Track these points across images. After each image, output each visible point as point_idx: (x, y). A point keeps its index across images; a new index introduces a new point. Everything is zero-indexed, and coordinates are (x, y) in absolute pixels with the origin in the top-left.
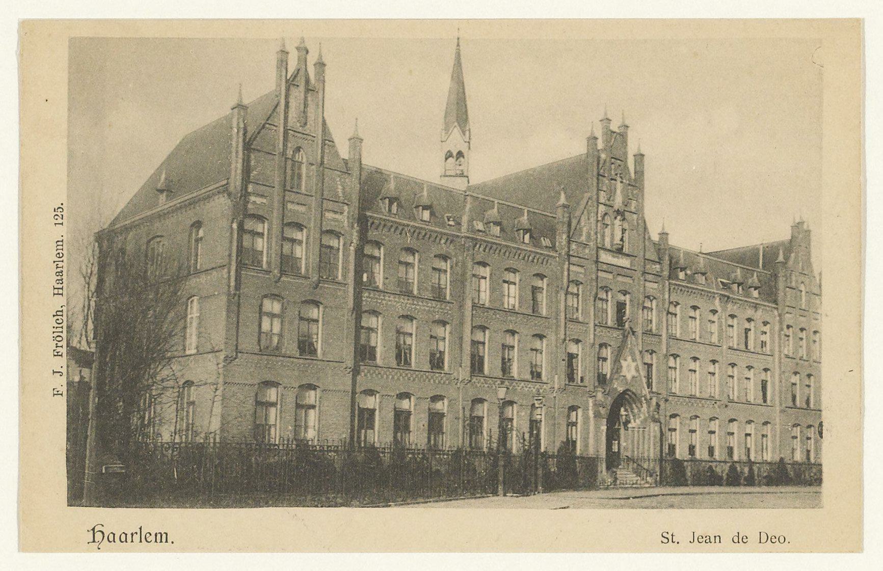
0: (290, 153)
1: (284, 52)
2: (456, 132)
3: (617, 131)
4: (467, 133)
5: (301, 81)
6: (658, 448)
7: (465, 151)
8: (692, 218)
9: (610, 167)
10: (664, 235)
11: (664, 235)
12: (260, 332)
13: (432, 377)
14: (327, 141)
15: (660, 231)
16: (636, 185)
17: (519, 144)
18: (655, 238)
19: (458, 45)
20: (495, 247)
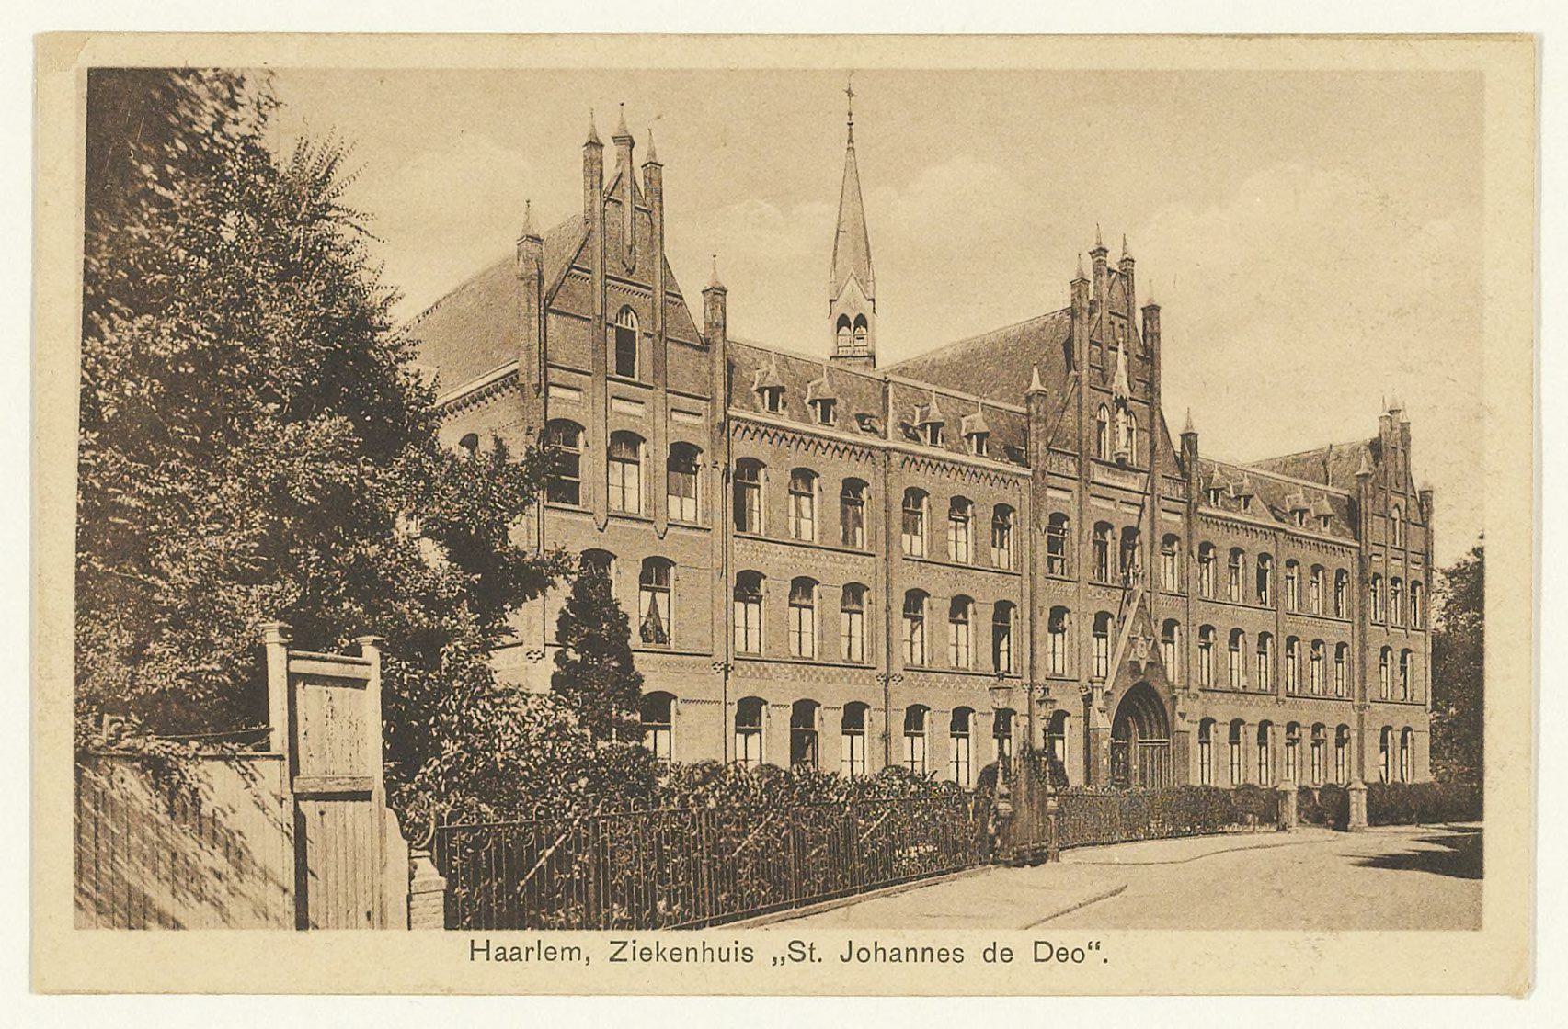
0: (612, 315)
1: (594, 144)
8: (1248, 405)
9: (1106, 339)
10: (1189, 439)
14: (674, 298)
17: (959, 296)
19: (850, 141)
20: (807, 439)
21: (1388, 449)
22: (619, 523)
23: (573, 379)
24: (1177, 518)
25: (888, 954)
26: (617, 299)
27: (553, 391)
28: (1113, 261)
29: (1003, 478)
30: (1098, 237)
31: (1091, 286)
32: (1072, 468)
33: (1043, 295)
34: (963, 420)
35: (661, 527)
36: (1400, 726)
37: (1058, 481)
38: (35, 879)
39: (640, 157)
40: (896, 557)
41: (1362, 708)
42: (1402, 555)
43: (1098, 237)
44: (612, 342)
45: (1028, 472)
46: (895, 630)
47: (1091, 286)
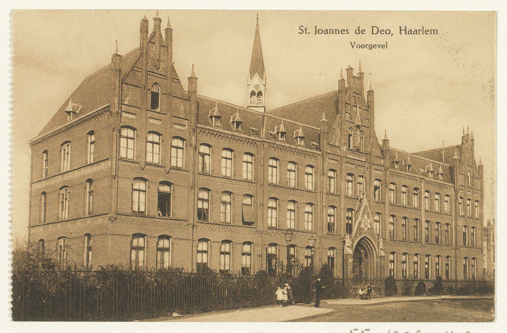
2: (256, 78)
3: (357, 76)
4: (264, 79)
5: (156, 40)
6: (345, 264)
7: (262, 89)
9: (351, 100)
10: (385, 141)
11: (385, 141)
12: (343, 255)
13: (227, 228)
14: (175, 79)
15: (383, 139)
16: (369, 108)
17: (301, 76)
18: (381, 143)
19: (257, 25)
22: (175, 171)
23: (132, 110)
24: (380, 173)
26: (152, 79)
27: (124, 115)
28: (355, 73)
31: (346, 82)
33: (328, 85)
34: (295, 132)
35: (167, 170)
38: (493, 193)
41: (456, 249)
44: (150, 96)
47: (346, 82)
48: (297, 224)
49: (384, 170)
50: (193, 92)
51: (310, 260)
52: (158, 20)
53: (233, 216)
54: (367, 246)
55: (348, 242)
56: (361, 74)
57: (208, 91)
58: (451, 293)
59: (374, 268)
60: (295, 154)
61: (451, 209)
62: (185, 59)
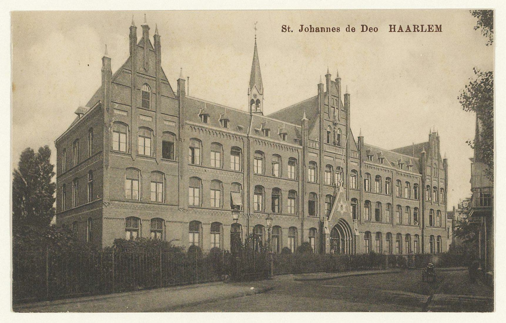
9: (328, 105)
14: (166, 82)
21: (434, 138)
25: (315, 30)
28: (333, 78)
29: (292, 149)
30: (328, 70)
32: (317, 146)
36: (436, 236)
37: (311, 150)
39: (152, 33)
40: (252, 175)
42: (437, 179)
43: (328, 70)
45: (301, 147)
46: (251, 199)
48: (201, 200)
49: (319, 153)
50: (181, 91)
51: (293, 239)
52: (146, 28)
53: (222, 201)
54: (344, 228)
55: (326, 224)
56: (338, 80)
57: (195, 91)
58: (327, 271)
59: (274, 246)
60: (219, 135)
61: (243, 166)
62: (173, 64)
